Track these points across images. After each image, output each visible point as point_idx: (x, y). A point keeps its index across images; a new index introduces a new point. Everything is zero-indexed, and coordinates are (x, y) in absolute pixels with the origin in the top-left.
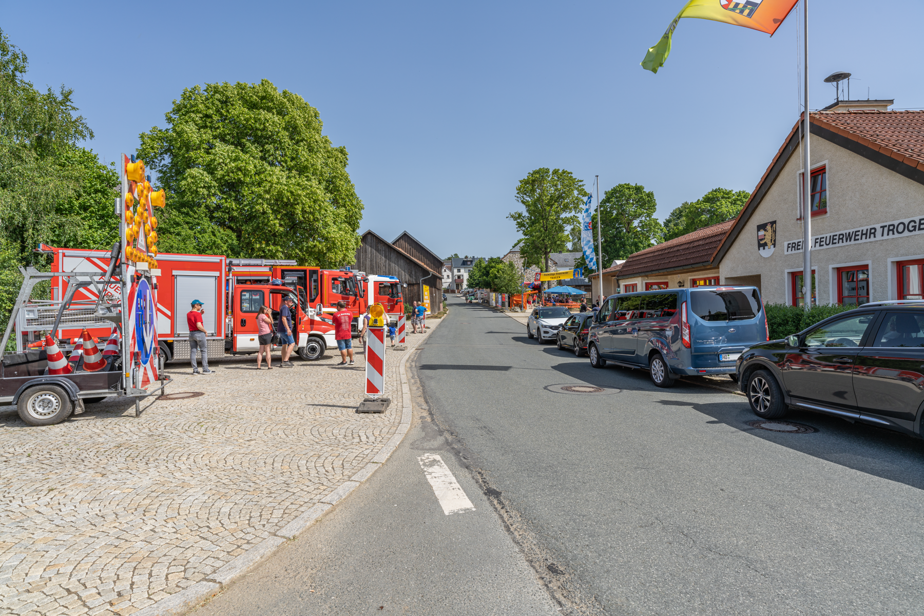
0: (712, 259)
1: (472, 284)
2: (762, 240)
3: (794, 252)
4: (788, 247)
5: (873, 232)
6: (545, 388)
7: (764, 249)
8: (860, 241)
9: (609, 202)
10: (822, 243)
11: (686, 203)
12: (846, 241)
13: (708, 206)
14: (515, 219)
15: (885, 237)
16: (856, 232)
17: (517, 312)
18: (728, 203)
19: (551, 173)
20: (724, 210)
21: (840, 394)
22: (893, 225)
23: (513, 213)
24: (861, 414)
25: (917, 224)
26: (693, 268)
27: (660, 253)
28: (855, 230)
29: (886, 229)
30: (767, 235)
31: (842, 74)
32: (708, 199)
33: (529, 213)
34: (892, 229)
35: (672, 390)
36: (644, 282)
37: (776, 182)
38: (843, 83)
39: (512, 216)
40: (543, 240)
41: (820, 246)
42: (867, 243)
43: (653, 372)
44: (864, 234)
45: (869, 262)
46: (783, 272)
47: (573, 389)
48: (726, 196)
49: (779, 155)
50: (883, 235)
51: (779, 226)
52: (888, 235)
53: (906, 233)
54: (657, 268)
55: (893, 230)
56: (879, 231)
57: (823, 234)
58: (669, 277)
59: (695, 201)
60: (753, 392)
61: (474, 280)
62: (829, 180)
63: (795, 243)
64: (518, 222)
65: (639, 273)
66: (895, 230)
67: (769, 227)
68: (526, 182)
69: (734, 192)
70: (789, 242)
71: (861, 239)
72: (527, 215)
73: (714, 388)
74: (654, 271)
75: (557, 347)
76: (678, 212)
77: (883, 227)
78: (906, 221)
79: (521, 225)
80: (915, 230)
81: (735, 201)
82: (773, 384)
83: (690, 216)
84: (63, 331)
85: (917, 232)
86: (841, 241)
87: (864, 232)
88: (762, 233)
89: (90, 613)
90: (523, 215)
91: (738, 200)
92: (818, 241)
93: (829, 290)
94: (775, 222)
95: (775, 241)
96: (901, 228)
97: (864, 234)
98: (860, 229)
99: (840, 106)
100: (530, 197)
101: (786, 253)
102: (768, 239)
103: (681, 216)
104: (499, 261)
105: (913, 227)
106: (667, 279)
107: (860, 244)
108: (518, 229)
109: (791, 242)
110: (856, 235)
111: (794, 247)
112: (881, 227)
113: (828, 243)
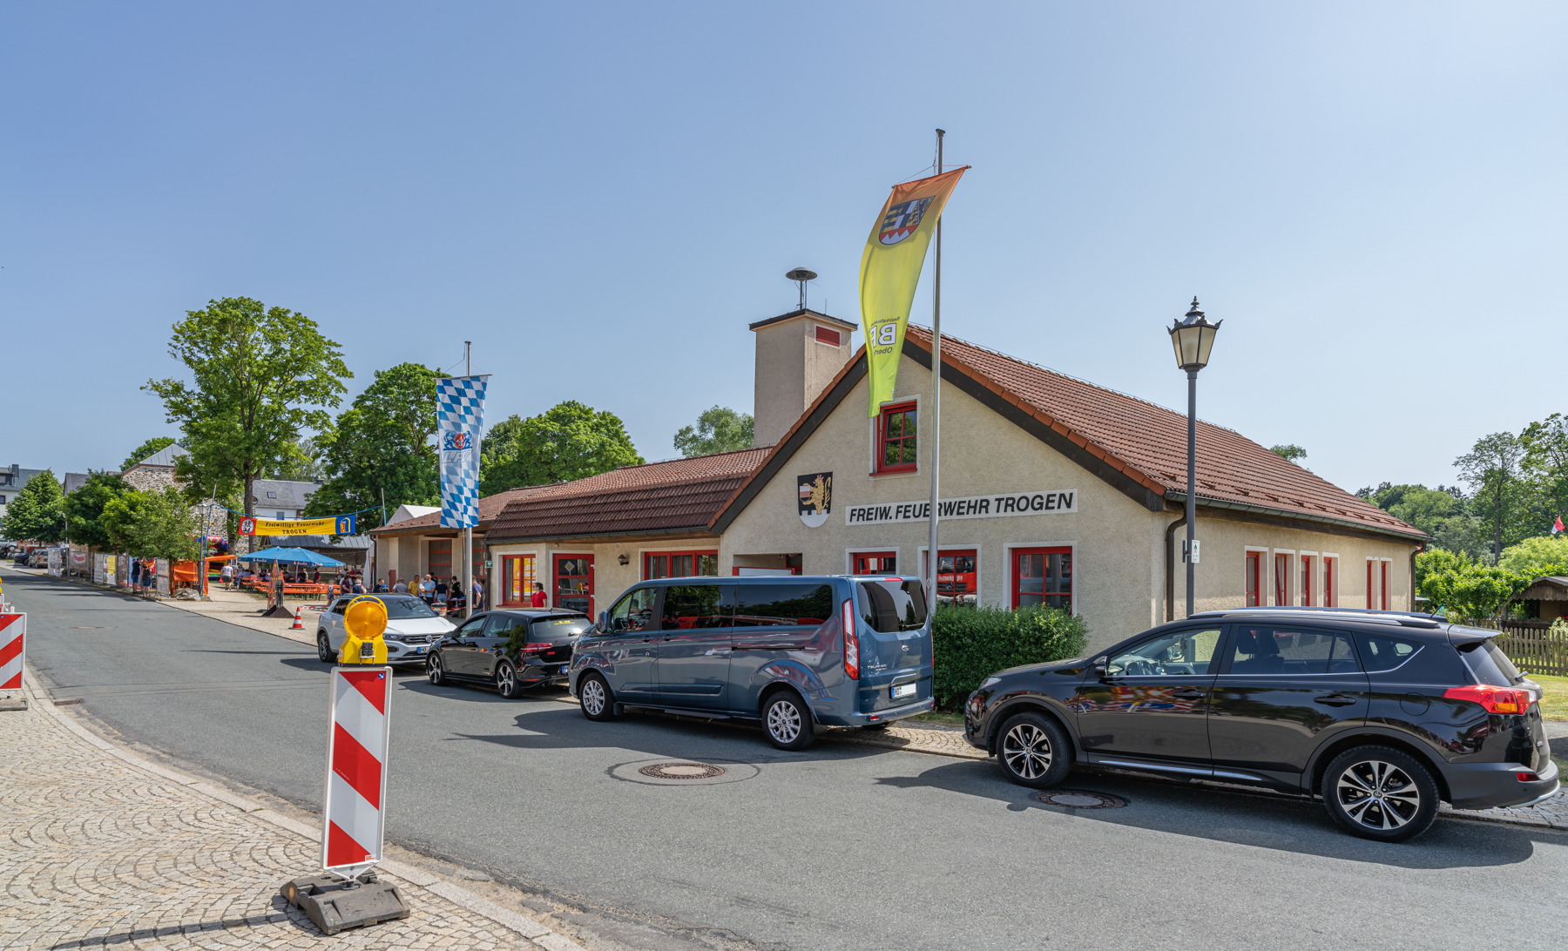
0: (713, 522)
1: (20, 529)
2: (806, 499)
3: (861, 522)
4: (852, 515)
5: (984, 505)
6: (610, 771)
7: (810, 513)
8: (965, 516)
9: (385, 393)
10: (907, 514)
11: (516, 417)
12: (946, 515)
13: (554, 427)
14: (165, 394)
15: (1002, 513)
16: (960, 502)
17: (192, 600)
18: (587, 428)
19: (266, 313)
20: (583, 438)
21: (1159, 742)
22: (1013, 499)
23: (159, 380)
24: (1213, 769)
25: (1045, 501)
26: (648, 535)
27: (585, 502)
28: (958, 500)
29: (1003, 503)
30: (818, 493)
31: (807, 272)
32: (556, 417)
33: (204, 388)
34: (1011, 504)
35: (808, 754)
36: (551, 552)
37: (1004, 422)
39: (156, 387)
40: (248, 450)
41: (905, 517)
42: (975, 519)
43: (771, 725)
44: (972, 507)
45: (978, 546)
46: (841, 552)
47: (665, 770)
48: (584, 415)
49: (845, 372)
50: (998, 511)
51: (837, 482)
52: (1005, 511)
53: (1030, 511)
54: (585, 529)
55: (1012, 506)
56: (993, 505)
57: (909, 500)
58: (596, 546)
59: (534, 416)
60: (1008, 747)
61: (27, 521)
62: (921, 424)
63: (864, 510)
64: (172, 403)
65: (544, 535)
66: (1015, 506)
67: (819, 481)
68: (204, 321)
69: (595, 412)
70: (854, 507)
71: (968, 513)
72: (198, 390)
73: (877, 746)
74: (579, 533)
76: (502, 430)
77: (999, 500)
78: (1030, 496)
79: (178, 409)
80: (1041, 508)
81: (597, 425)
82: (1054, 730)
83: (528, 440)
85: (1044, 511)
87: (972, 504)
88: (806, 488)
90: (187, 389)
91: (602, 425)
92: (903, 509)
94: (830, 474)
95: (829, 503)
96: (1023, 504)
97: (972, 507)
98: (967, 499)
99: (806, 317)
100: (207, 352)
101: (848, 523)
102: (816, 499)
103: (507, 439)
104: (115, 483)
105: (1038, 504)
106: (593, 549)
107: (966, 520)
108: (171, 417)
109: (858, 507)
110: (959, 507)
111: (863, 515)
112: (996, 500)
113: (917, 514)
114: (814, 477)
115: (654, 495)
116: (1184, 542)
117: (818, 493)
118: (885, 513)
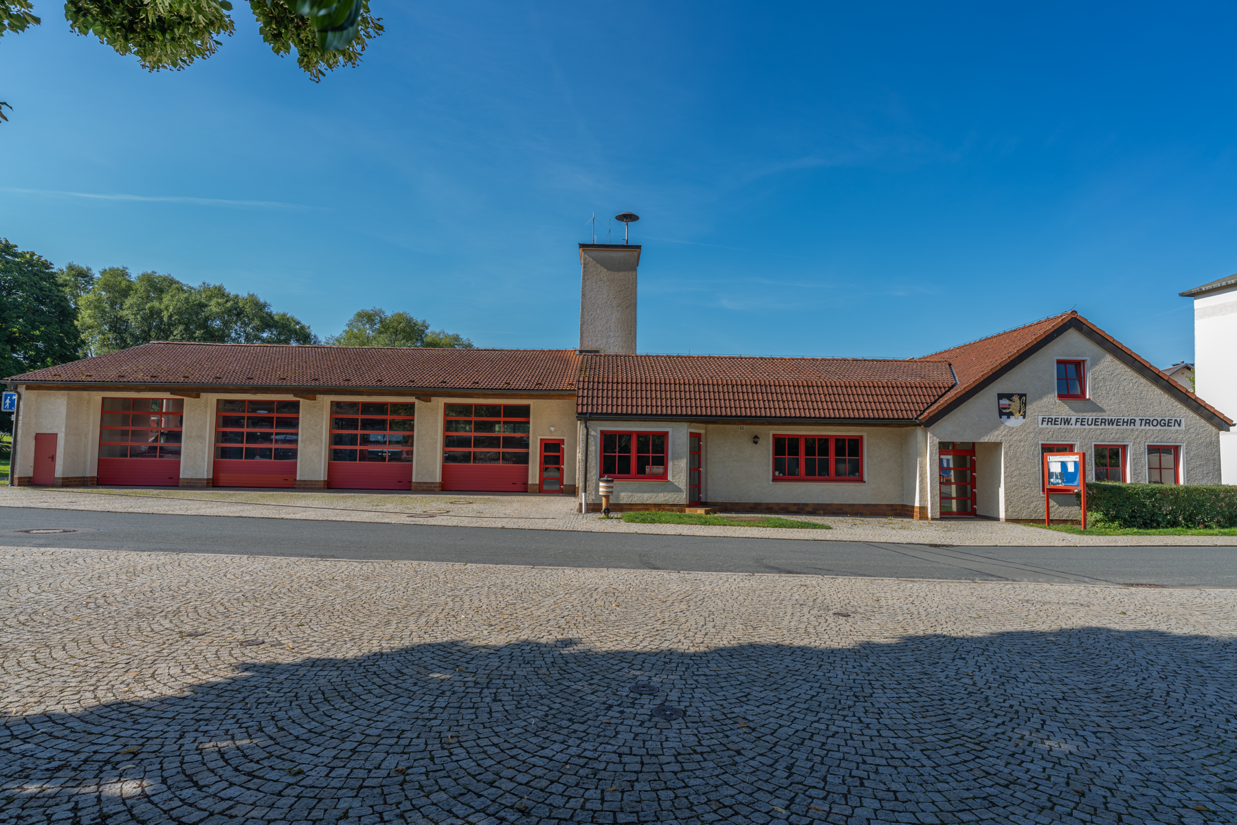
4: (1076, 421)
5: (1133, 422)
15: (1143, 427)
29: (1144, 422)
34: (1148, 422)
38: (219, 46)
53: (1159, 426)
56: (1138, 422)
67: (1016, 398)
77: (1142, 420)
86: (1125, 424)
88: (1004, 402)
89: (980, 823)
94: (1025, 395)
96: (1155, 423)
101: (1040, 426)
113: (1090, 423)
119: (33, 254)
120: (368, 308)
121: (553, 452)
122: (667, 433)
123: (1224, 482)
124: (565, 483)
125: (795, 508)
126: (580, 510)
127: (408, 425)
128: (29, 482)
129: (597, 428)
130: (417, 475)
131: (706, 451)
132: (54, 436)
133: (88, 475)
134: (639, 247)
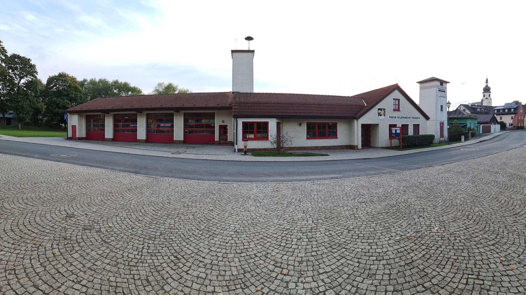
5: (410, 118)
33: (11, 57)
34: (413, 118)
56: (411, 118)
67: (383, 110)
75: (481, 132)
84: (268, 122)
88: (380, 111)
93: (323, 123)
94: (385, 109)
114: (381, 109)
115: (267, 105)
116: (442, 125)
117: (382, 113)
118: (395, 117)
119: (73, 76)
120: (161, 82)
121: (224, 129)
122: (268, 122)
123: (420, 134)
124: (228, 140)
125: (315, 148)
126: (235, 151)
127: (172, 121)
128: (69, 139)
129: (240, 121)
130: (175, 138)
131: (282, 129)
132: (75, 126)
133: (84, 137)
134: (253, 51)
